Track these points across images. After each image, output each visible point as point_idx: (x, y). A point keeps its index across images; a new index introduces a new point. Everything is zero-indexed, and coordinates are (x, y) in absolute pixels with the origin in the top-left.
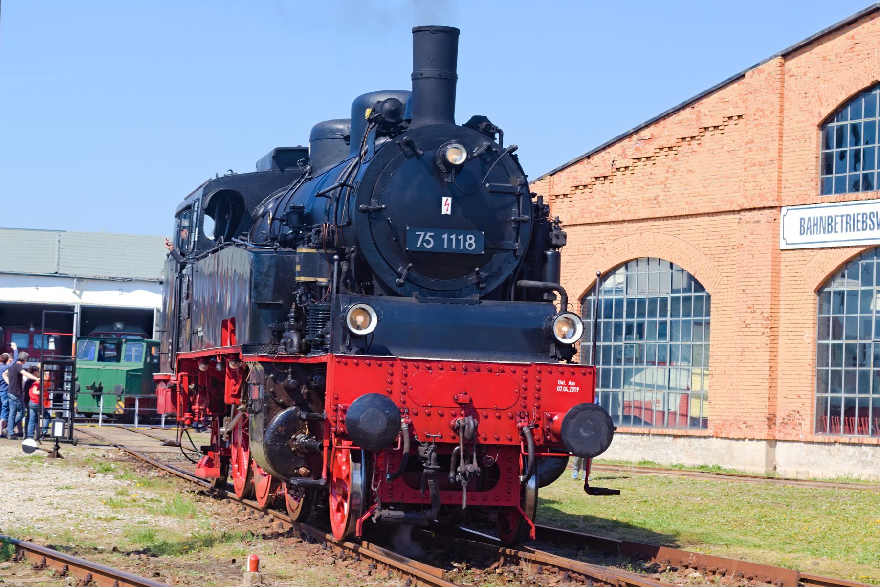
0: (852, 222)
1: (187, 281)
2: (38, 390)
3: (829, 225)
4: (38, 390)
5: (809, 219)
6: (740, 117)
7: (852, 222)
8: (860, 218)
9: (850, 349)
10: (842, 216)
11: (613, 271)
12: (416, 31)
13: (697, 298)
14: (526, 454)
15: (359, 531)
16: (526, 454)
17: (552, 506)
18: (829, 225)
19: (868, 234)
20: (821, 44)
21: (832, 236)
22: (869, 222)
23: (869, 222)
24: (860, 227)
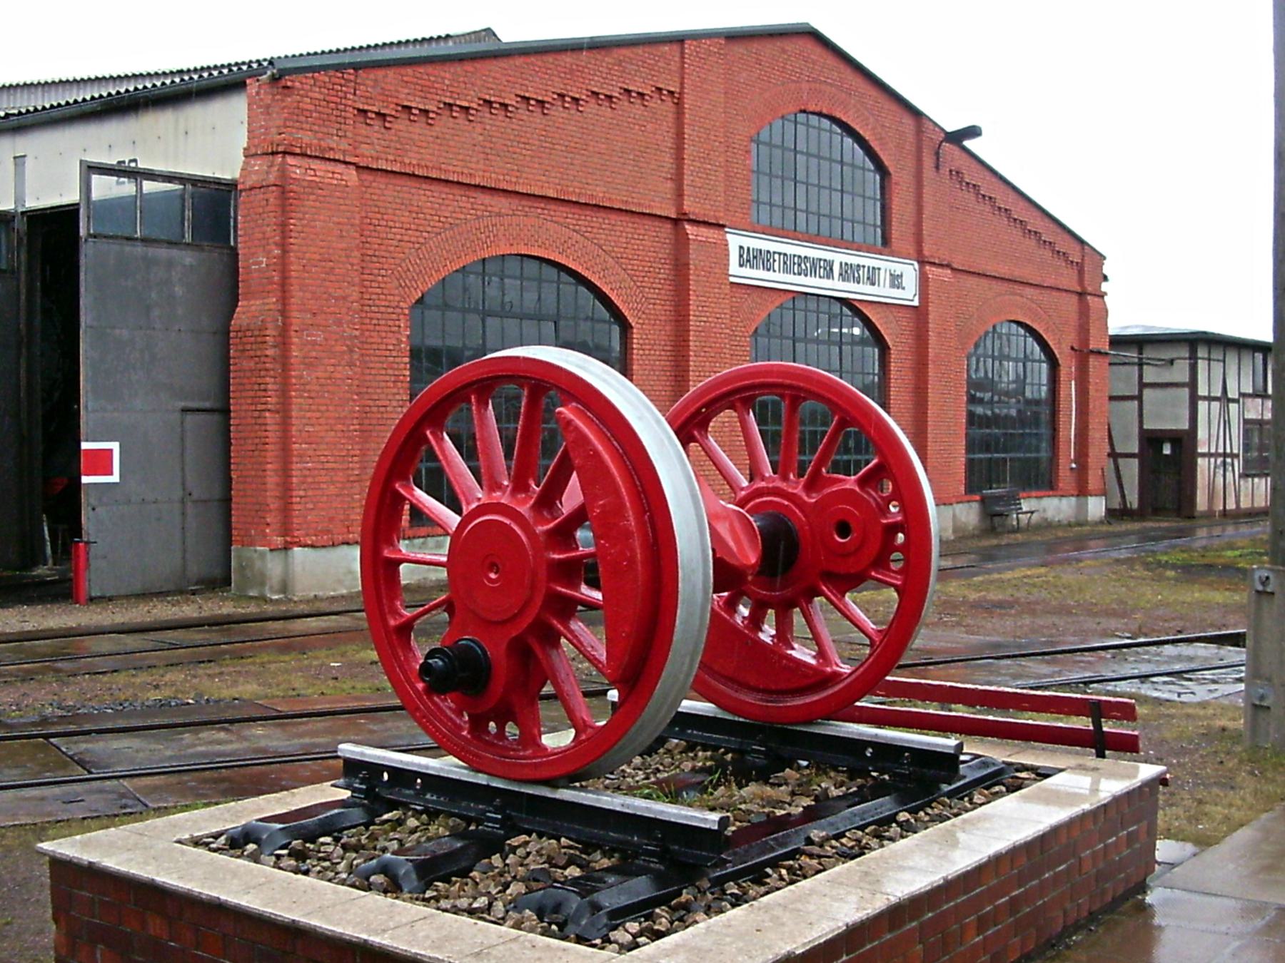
0: (790, 264)
7: (790, 264)
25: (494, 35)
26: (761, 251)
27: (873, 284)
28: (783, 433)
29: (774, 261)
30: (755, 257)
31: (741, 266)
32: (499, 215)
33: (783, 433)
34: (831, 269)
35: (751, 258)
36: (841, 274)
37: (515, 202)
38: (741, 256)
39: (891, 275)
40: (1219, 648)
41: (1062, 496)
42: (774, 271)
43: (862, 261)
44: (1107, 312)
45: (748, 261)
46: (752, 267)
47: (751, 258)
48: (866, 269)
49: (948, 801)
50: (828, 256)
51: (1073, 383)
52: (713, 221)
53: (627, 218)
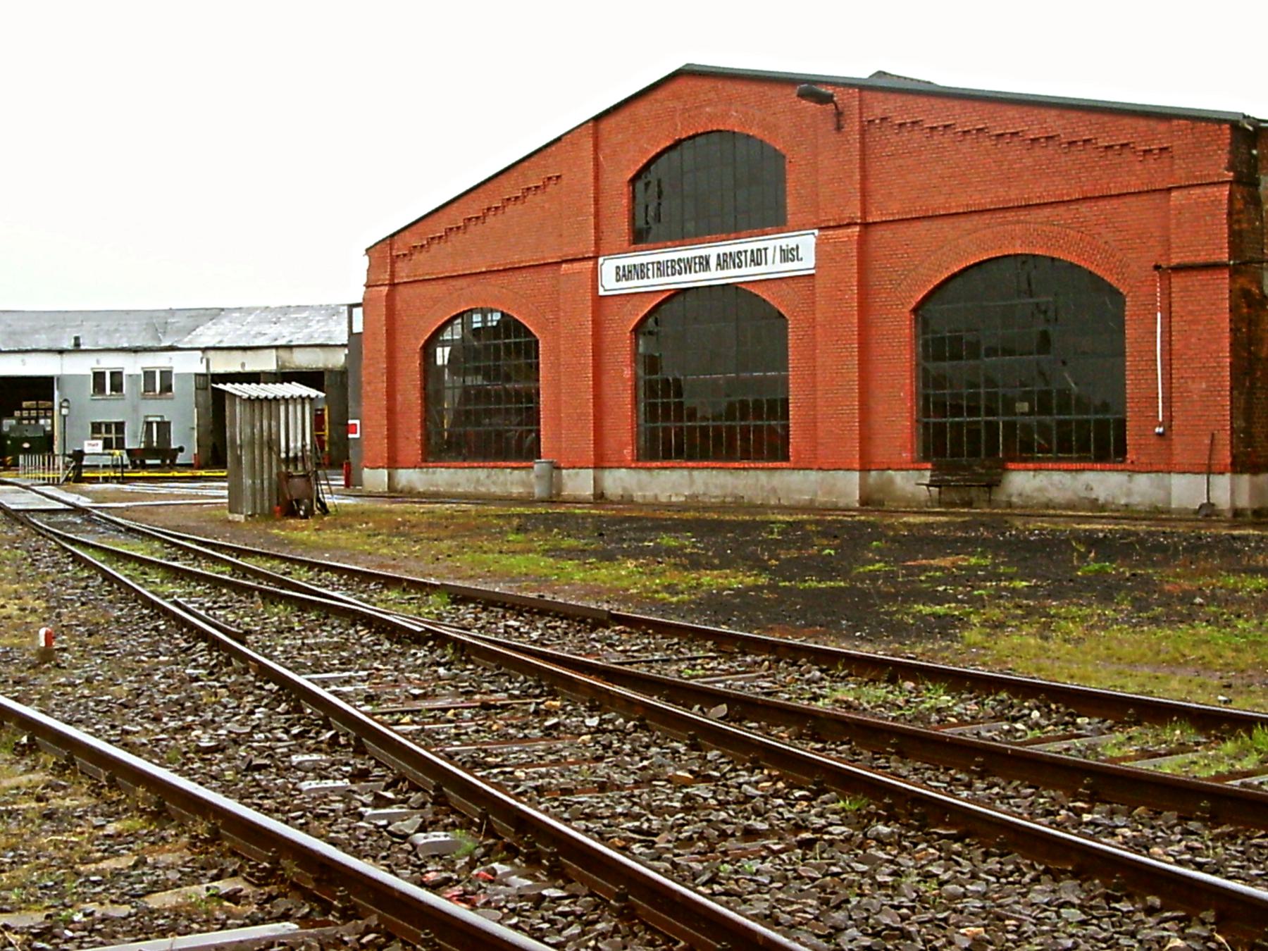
0: (661, 269)
1: (695, 654)
2: (10, 427)
3: (641, 271)
4: (10, 427)
5: (624, 267)
6: (558, 177)
7: (661, 269)
8: (669, 264)
9: (666, 417)
10: (653, 263)
11: (450, 322)
12: (367, 250)
13: (526, 343)
14: (983, 352)
15: (645, 414)
16: (983, 352)
17: (133, 939)
18: (641, 271)
19: (677, 278)
20: (241, 942)
21: (645, 282)
22: (677, 267)
23: (677, 267)
24: (670, 272)
25: (885, 73)
26: (635, 266)
27: (759, 264)
28: (1246, 519)
29: (648, 269)
30: (630, 272)
31: (618, 281)
32: (462, 289)
33: (1246, 519)
34: (708, 263)
35: (623, 274)
36: (719, 264)
37: (468, 280)
38: (617, 273)
39: (782, 250)
40: (836, 502)
41: (1134, 471)
42: (648, 278)
43: (741, 247)
44: (368, 270)
45: (624, 276)
46: (627, 280)
47: (624, 274)
48: (749, 254)
49: (807, 687)
50: (703, 252)
51: (1159, 315)
52: (580, 256)
53: (532, 270)
